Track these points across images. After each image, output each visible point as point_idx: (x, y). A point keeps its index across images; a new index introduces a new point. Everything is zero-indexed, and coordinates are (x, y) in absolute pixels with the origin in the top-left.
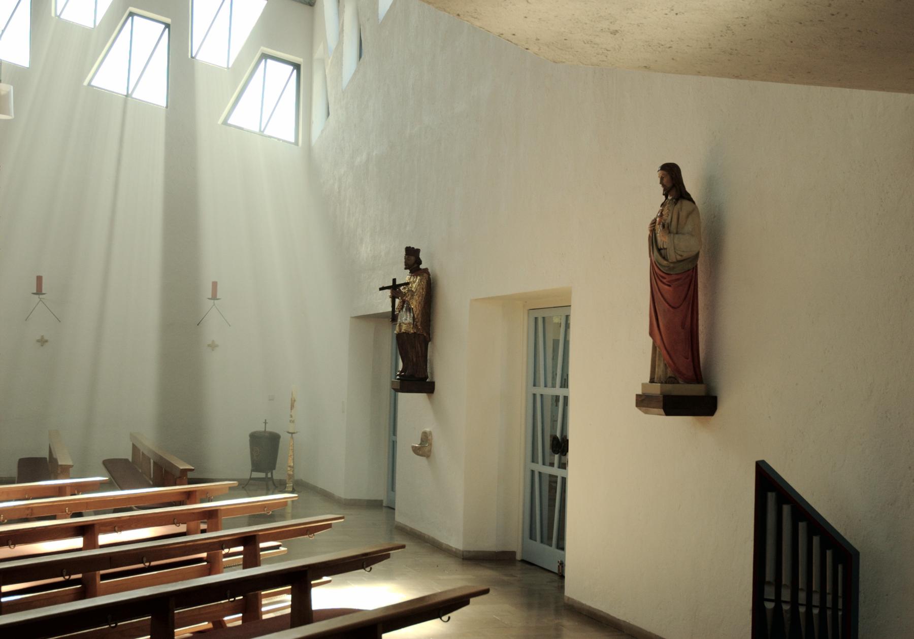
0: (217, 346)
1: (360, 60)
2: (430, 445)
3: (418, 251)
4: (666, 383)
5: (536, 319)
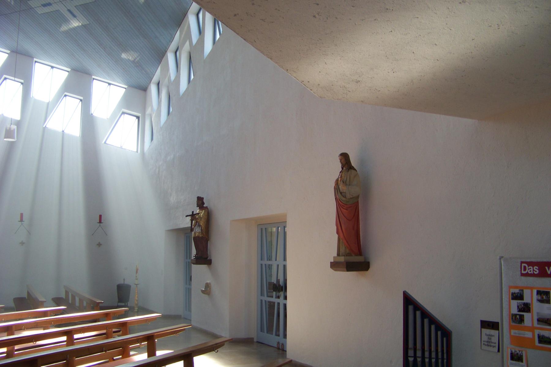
1: (168, 115)
2: (210, 289)
3: (203, 198)
4: (347, 256)
5: (262, 229)
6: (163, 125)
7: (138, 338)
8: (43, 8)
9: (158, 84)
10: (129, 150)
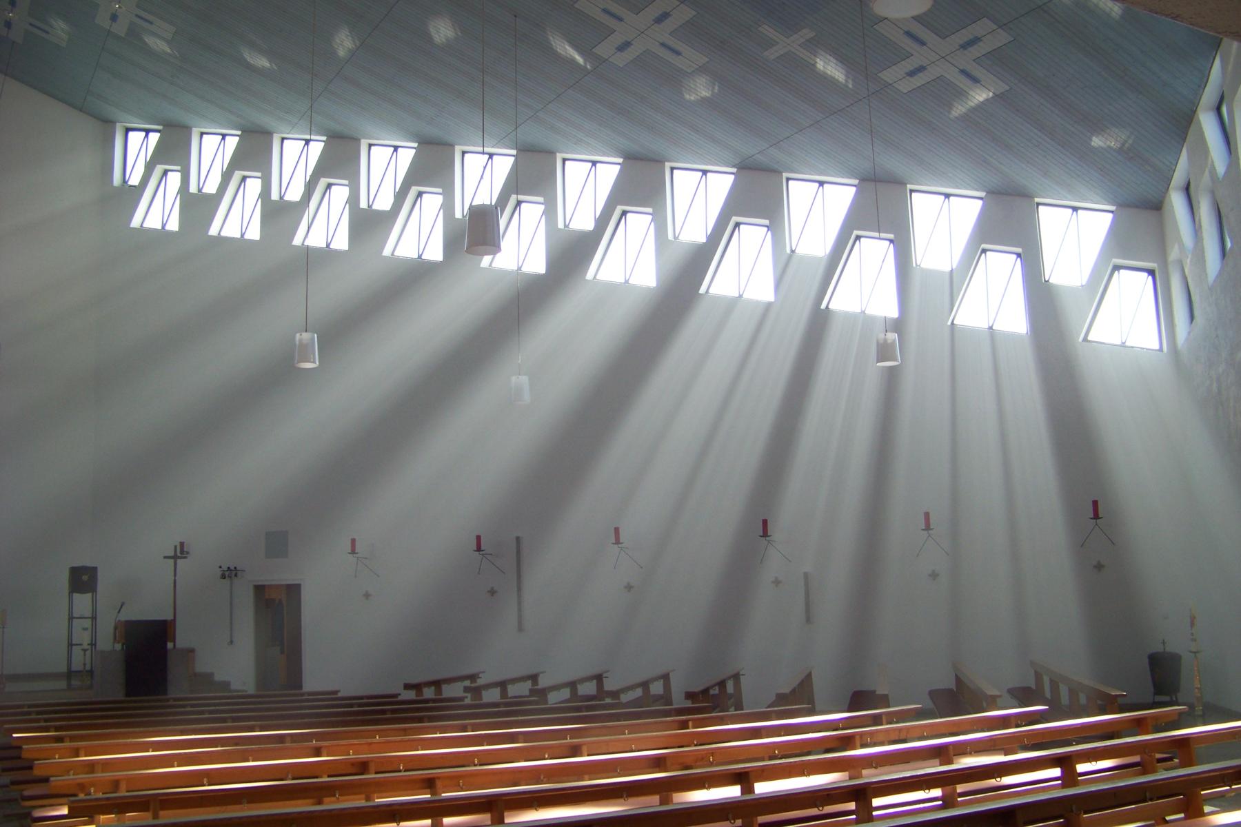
0: (496, 592)
6: (1215, 281)
7: (1222, 772)
8: (911, 79)
9: (1187, 189)
10: (1141, 348)
